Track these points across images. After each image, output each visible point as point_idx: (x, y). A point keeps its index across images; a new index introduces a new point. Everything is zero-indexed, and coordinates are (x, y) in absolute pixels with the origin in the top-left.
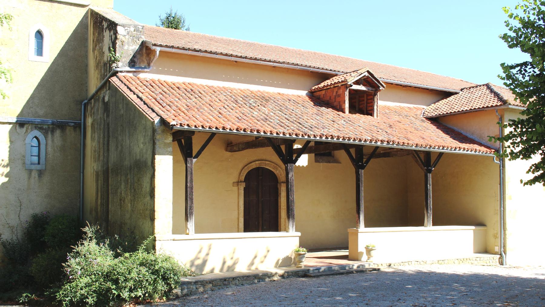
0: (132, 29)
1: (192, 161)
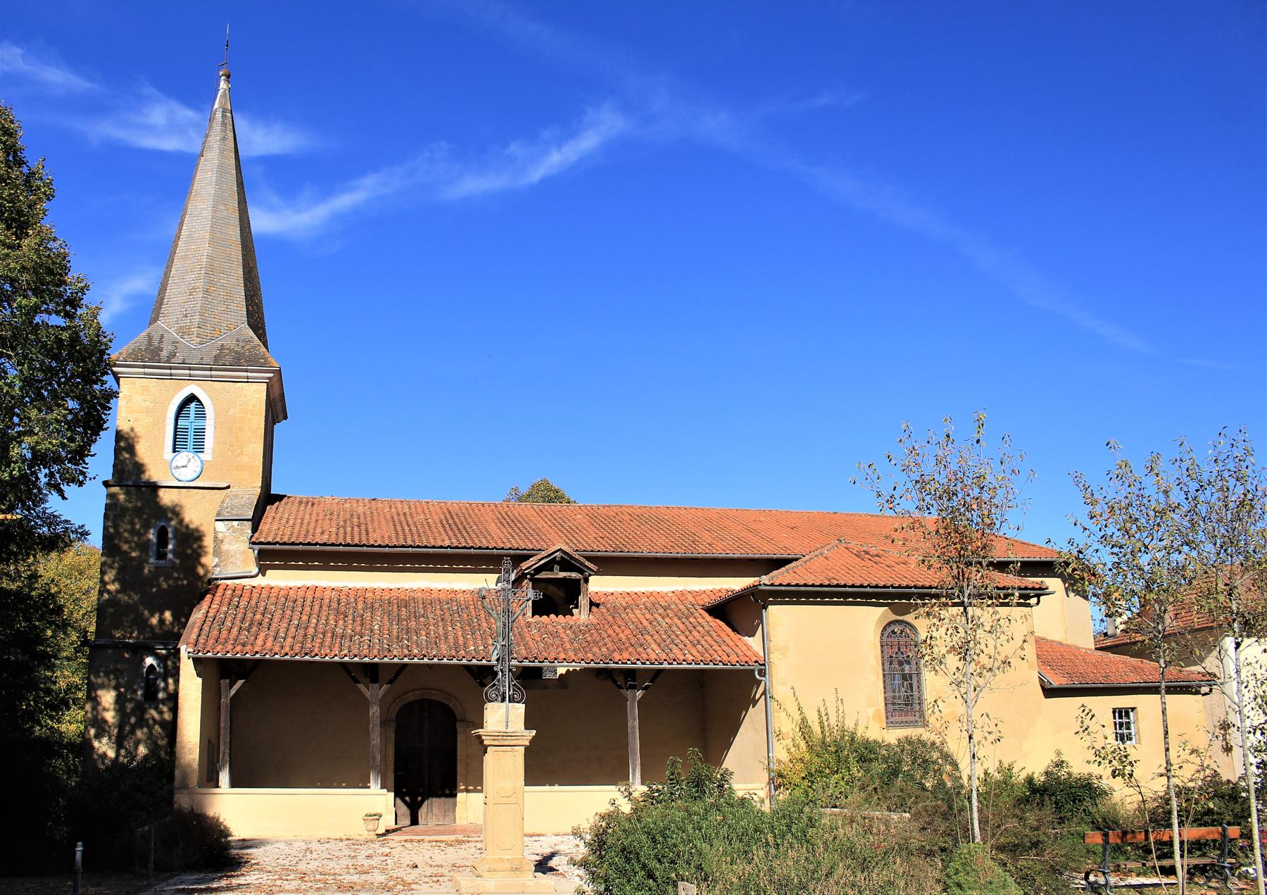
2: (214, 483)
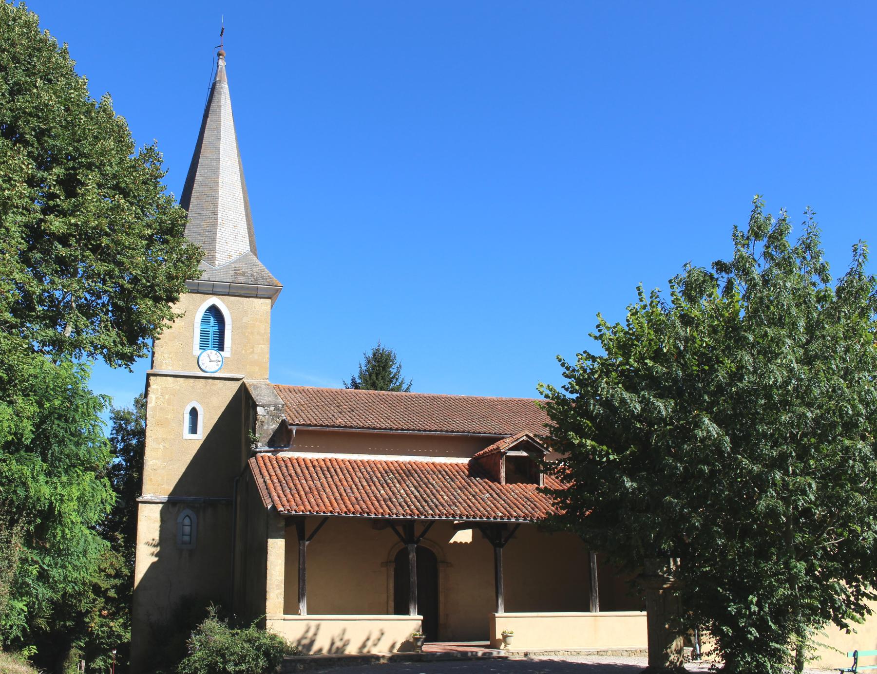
0: (272, 408)
1: (304, 544)
2: (233, 375)
